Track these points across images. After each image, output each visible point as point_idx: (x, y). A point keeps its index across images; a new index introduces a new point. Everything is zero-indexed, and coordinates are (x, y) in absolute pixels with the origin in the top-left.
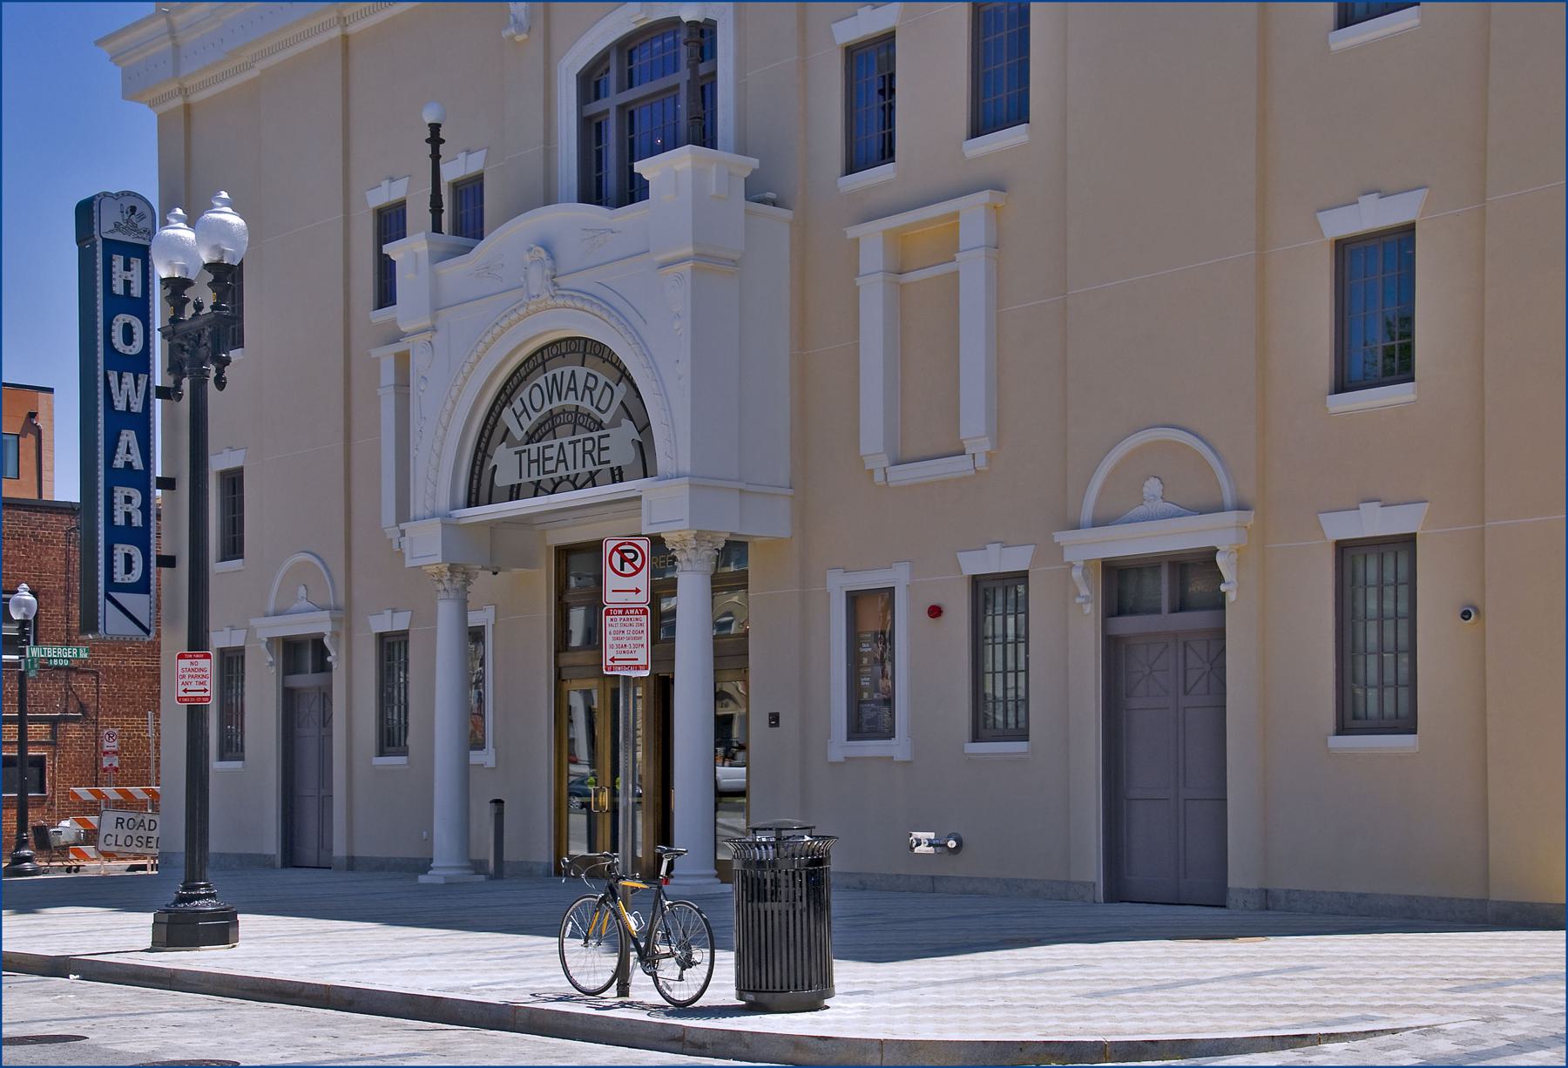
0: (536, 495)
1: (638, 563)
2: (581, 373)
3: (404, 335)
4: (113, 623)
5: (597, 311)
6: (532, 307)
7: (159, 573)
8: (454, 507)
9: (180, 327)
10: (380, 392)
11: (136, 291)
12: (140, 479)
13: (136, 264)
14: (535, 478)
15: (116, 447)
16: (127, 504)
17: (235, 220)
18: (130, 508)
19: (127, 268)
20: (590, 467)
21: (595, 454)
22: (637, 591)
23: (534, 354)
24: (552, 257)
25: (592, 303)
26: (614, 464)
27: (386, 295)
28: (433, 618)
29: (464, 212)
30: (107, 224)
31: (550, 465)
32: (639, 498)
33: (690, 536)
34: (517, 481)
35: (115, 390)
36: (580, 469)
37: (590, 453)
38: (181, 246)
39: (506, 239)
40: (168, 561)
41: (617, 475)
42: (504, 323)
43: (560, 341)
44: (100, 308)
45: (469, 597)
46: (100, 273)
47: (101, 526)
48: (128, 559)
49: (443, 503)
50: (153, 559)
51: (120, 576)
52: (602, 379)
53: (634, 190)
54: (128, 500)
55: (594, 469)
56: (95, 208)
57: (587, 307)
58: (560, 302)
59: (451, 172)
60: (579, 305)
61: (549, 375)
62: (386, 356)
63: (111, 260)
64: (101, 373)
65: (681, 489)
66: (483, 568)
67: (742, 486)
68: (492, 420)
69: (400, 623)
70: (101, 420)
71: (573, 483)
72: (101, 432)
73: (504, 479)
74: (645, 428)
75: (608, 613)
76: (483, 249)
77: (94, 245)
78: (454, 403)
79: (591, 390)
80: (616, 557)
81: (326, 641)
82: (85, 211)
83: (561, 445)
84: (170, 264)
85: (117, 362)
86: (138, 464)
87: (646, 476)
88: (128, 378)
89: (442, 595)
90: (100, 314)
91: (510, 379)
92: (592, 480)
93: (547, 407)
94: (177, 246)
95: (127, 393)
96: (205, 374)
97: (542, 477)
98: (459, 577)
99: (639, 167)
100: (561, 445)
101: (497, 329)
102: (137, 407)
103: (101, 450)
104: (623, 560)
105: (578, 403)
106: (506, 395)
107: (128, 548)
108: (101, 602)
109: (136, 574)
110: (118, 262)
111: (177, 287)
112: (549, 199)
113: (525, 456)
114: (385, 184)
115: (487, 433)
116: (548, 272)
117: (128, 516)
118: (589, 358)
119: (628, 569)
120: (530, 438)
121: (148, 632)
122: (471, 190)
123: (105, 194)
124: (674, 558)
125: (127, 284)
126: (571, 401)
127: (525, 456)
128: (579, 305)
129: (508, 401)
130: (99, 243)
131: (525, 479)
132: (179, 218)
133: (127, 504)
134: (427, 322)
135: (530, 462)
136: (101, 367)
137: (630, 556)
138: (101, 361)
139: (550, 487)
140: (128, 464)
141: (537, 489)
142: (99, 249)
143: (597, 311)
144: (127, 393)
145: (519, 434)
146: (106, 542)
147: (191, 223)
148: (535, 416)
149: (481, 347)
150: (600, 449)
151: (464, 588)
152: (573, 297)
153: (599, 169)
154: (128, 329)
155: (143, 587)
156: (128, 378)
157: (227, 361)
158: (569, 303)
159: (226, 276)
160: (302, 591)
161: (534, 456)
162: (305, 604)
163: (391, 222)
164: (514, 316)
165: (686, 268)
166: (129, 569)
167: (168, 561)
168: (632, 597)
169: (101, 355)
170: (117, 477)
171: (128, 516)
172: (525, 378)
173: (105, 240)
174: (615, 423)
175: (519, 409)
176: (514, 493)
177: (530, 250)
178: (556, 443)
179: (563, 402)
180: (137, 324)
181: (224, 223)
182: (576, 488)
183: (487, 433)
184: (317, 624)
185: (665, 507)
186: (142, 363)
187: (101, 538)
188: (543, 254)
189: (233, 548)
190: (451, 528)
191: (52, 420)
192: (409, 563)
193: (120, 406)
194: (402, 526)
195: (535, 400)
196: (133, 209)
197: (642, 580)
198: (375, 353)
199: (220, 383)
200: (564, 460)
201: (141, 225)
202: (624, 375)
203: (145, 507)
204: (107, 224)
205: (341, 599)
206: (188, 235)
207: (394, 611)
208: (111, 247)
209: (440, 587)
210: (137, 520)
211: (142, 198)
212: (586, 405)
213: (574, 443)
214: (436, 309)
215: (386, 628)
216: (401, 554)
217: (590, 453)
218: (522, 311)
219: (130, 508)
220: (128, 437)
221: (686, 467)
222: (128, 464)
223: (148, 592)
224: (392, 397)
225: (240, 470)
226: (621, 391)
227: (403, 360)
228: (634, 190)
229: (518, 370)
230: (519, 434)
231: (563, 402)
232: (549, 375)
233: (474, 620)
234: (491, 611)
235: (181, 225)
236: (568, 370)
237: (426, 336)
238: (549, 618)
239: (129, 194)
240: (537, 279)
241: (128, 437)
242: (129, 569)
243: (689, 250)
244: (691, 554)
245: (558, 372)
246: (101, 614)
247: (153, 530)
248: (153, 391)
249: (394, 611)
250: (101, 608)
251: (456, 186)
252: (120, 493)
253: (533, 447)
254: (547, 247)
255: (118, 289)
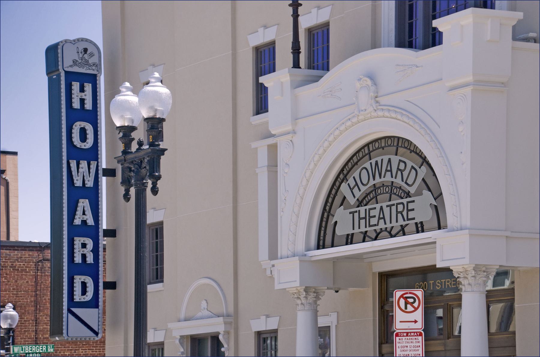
0: (364, 241)
1: (416, 305)
2: (395, 160)
3: (273, 136)
4: (74, 329)
5: (405, 119)
6: (361, 117)
7: (104, 293)
8: (308, 250)
9: (129, 157)
10: (258, 171)
11: (89, 106)
12: (92, 231)
13: (88, 87)
14: (363, 229)
15: (76, 210)
16: (83, 248)
17: (164, 90)
18: (85, 251)
19: (82, 90)
20: (401, 222)
21: (405, 213)
22: (416, 322)
23: (363, 147)
24: (375, 84)
25: (402, 114)
26: (418, 220)
27: (261, 105)
28: (294, 322)
29: (316, 53)
30: (68, 60)
31: (374, 221)
32: (435, 243)
33: (470, 268)
34: (353, 232)
35: (74, 173)
36: (394, 224)
37: (401, 213)
38: (127, 106)
39: (345, 72)
40: (111, 285)
41: (420, 228)
42: (342, 128)
43: (381, 139)
44: (64, 118)
45: (319, 308)
46: (63, 94)
47: (65, 264)
48: (84, 285)
49: (301, 247)
50: (101, 285)
51: (78, 297)
52: (410, 164)
53: (434, 39)
54: (84, 246)
55: (404, 223)
56: (60, 51)
57: (399, 117)
58: (380, 113)
59: (306, 22)
60: (393, 115)
61: (373, 161)
62: (262, 147)
63: (71, 85)
64: (65, 162)
65: (464, 236)
66: (328, 289)
67: (508, 234)
68: (334, 192)
69: (272, 324)
70: (65, 193)
71: (390, 233)
72: (65, 201)
73: (342, 231)
74: (439, 196)
75: (397, 335)
76: (329, 78)
77: (59, 76)
78: (308, 181)
79: (402, 171)
80: (402, 302)
81: (221, 337)
82: (53, 53)
83: (381, 208)
84: (122, 117)
85: (75, 153)
86: (91, 222)
87: (439, 228)
88: (84, 164)
89: (300, 307)
90: (64, 122)
91: (346, 164)
92: (403, 231)
93: (372, 182)
94: (126, 107)
95: (83, 174)
96: (145, 185)
97: (368, 229)
98: (312, 295)
99: (436, 23)
100: (381, 208)
101: (337, 132)
102: (90, 183)
103: (65, 213)
104: (406, 303)
105: (393, 180)
106: (343, 175)
107: (83, 278)
108: (65, 315)
109: (89, 296)
110: (76, 86)
111: (127, 132)
112: (375, 45)
113: (356, 215)
114: (261, 30)
115: (330, 200)
116: (372, 94)
117: (84, 256)
118: (401, 150)
119: (410, 308)
120: (360, 203)
121: (97, 334)
122: (320, 36)
123: (66, 41)
124: (460, 283)
125: (82, 101)
126: (388, 178)
127: (356, 215)
128: (393, 115)
129: (345, 179)
130: (63, 75)
131: (357, 230)
132: (128, 89)
133: (83, 248)
134: (289, 128)
135: (360, 219)
136: (65, 158)
137: (411, 300)
138: (65, 154)
139: (374, 235)
140: (84, 222)
141: (365, 237)
142: (63, 78)
143: (405, 119)
144: (83, 174)
145: (352, 201)
146: (69, 271)
147: (136, 91)
148: (363, 189)
149: (326, 144)
150: (408, 210)
151: (315, 302)
152: (389, 110)
153: (411, 17)
154: (83, 132)
155: (94, 303)
156: (84, 164)
157: (159, 177)
158: (387, 114)
159: (155, 125)
160: (204, 304)
161: (363, 215)
162: (206, 313)
163: (265, 59)
164: (349, 123)
165: (468, 90)
166: (84, 292)
167: (111, 285)
168: (412, 325)
169: (64, 150)
170: (75, 231)
171: (84, 256)
172: (356, 163)
173: (66, 72)
174: (419, 193)
175: (352, 184)
176: (349, 240)
177: (360, 80)
178: (378, 206)
179: (383, 179)
180: (89, 128)
181: (156, 93)
182: (392, 236)
183: (330, 200)
184: (215, 326)
185: (450, 250)
186: (93, 154)
187: (65, 272)
188: (369, 82)
189: (159, 277)
190: (304, 260)
191: (17, 175)
192: (277, 287)
193: (78, 183)
194: (273, 262)
195: (363, 178)
196: (86, 50)
197: (419, 315)
198: (254, 145)
199: (155, 191)
200: (384, 218)
201: (91, 61)
202: (425, 161)
203: (95, 251)
204: (68, 60)
205: (231, 310)
206: (133, 99)
207: (268, 316)
208: (71, 76)
209: (299, 302)
210: (90, 259)
211: (91, 42)
212: (398, 181)
213: (390, 206)
214: (295, 119)
215: (262, 328)
216: (272, 278)
217: (401, 213)
218: (355, 120)
219: (85, 251)
220: (84, 204)
221: (467, 222)
222: (84, 222)
223: (97, 306)
224: (266, 173)
225: (161, 223)
226: (423, 171)
227: (273, 150)
228: (434, 39)
229: (349, 161)
230: (352, 201)
231: (383, 179)
232: (373, 161)
233: (322, 322)
234: (334, 316)
235: (129, 93)
236: (386, 158)
237: (289, 137)
238: (374, 320)
239: (82, 40)
240: (365, 98)
241: (84, 204)
242: (84, 292)
243: (470, 79)
244: (471, 280)
245: (379, 159)
246: (65, 323)
247: (101, 269)
248: (100, 172)
249: (268, 316)
250: (65, 319)
251: (310, 31)
252: (78, 241)
253: (362, 209)
254: (371, 77)
255: (76, 105)
